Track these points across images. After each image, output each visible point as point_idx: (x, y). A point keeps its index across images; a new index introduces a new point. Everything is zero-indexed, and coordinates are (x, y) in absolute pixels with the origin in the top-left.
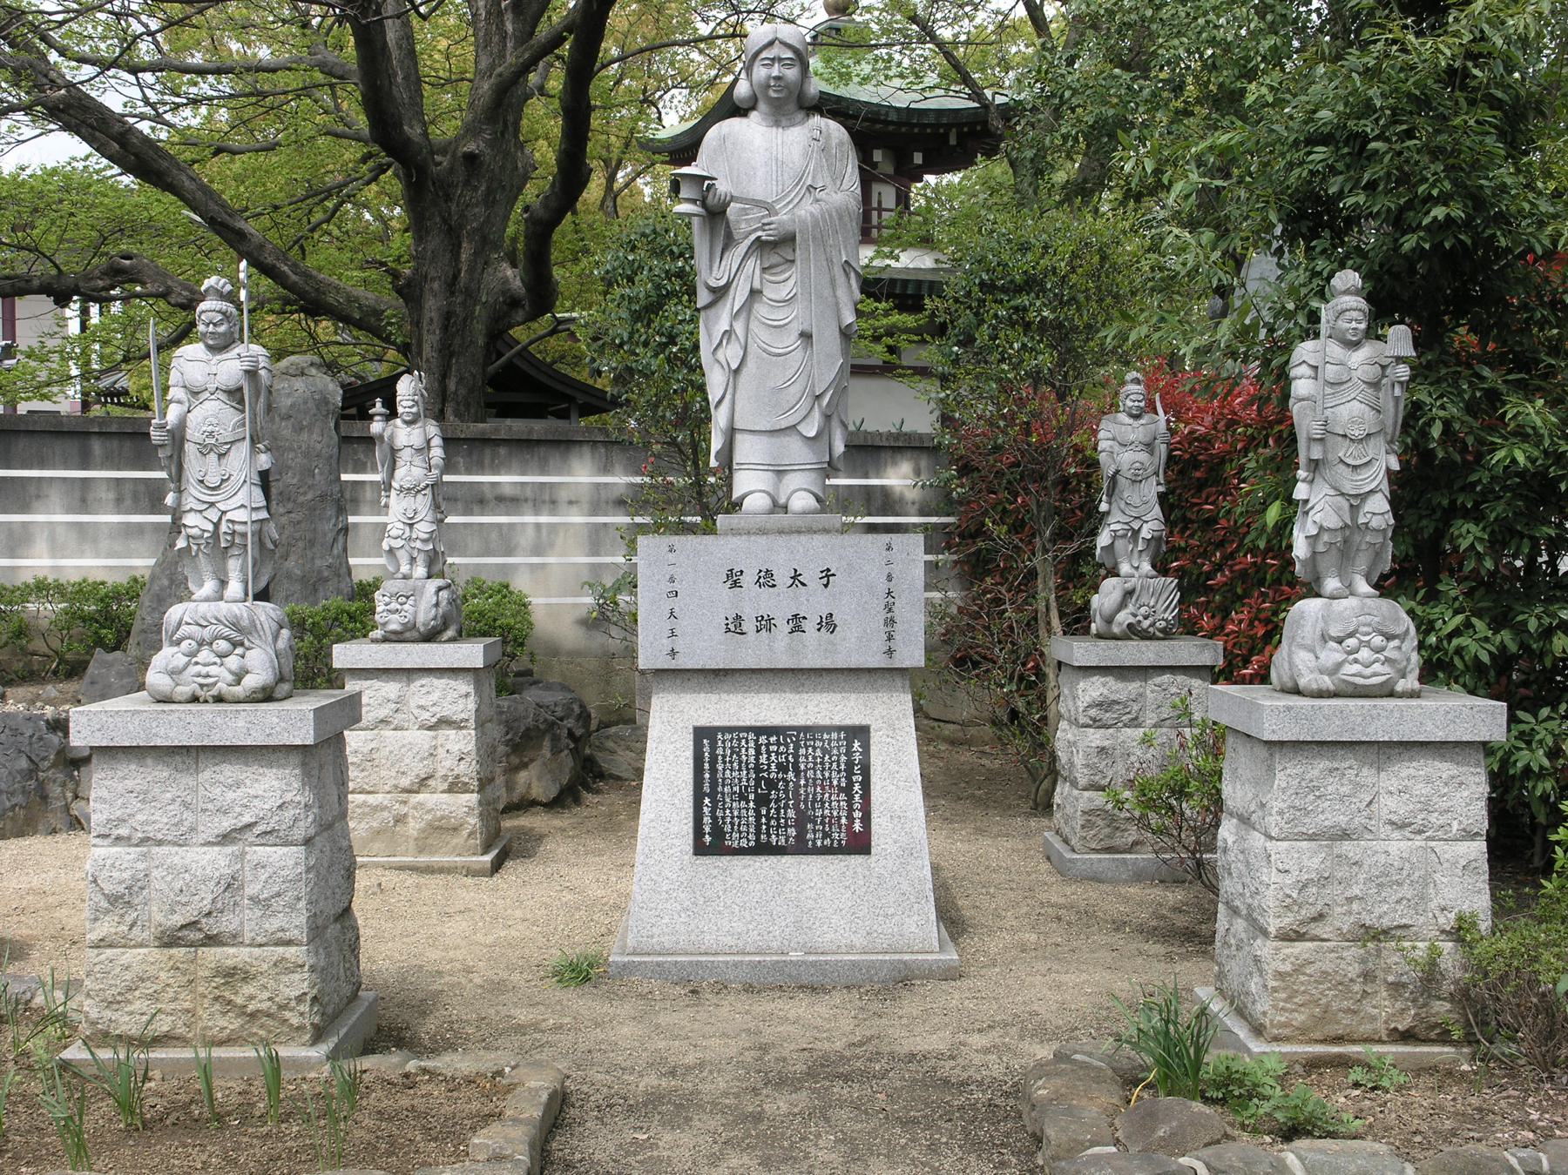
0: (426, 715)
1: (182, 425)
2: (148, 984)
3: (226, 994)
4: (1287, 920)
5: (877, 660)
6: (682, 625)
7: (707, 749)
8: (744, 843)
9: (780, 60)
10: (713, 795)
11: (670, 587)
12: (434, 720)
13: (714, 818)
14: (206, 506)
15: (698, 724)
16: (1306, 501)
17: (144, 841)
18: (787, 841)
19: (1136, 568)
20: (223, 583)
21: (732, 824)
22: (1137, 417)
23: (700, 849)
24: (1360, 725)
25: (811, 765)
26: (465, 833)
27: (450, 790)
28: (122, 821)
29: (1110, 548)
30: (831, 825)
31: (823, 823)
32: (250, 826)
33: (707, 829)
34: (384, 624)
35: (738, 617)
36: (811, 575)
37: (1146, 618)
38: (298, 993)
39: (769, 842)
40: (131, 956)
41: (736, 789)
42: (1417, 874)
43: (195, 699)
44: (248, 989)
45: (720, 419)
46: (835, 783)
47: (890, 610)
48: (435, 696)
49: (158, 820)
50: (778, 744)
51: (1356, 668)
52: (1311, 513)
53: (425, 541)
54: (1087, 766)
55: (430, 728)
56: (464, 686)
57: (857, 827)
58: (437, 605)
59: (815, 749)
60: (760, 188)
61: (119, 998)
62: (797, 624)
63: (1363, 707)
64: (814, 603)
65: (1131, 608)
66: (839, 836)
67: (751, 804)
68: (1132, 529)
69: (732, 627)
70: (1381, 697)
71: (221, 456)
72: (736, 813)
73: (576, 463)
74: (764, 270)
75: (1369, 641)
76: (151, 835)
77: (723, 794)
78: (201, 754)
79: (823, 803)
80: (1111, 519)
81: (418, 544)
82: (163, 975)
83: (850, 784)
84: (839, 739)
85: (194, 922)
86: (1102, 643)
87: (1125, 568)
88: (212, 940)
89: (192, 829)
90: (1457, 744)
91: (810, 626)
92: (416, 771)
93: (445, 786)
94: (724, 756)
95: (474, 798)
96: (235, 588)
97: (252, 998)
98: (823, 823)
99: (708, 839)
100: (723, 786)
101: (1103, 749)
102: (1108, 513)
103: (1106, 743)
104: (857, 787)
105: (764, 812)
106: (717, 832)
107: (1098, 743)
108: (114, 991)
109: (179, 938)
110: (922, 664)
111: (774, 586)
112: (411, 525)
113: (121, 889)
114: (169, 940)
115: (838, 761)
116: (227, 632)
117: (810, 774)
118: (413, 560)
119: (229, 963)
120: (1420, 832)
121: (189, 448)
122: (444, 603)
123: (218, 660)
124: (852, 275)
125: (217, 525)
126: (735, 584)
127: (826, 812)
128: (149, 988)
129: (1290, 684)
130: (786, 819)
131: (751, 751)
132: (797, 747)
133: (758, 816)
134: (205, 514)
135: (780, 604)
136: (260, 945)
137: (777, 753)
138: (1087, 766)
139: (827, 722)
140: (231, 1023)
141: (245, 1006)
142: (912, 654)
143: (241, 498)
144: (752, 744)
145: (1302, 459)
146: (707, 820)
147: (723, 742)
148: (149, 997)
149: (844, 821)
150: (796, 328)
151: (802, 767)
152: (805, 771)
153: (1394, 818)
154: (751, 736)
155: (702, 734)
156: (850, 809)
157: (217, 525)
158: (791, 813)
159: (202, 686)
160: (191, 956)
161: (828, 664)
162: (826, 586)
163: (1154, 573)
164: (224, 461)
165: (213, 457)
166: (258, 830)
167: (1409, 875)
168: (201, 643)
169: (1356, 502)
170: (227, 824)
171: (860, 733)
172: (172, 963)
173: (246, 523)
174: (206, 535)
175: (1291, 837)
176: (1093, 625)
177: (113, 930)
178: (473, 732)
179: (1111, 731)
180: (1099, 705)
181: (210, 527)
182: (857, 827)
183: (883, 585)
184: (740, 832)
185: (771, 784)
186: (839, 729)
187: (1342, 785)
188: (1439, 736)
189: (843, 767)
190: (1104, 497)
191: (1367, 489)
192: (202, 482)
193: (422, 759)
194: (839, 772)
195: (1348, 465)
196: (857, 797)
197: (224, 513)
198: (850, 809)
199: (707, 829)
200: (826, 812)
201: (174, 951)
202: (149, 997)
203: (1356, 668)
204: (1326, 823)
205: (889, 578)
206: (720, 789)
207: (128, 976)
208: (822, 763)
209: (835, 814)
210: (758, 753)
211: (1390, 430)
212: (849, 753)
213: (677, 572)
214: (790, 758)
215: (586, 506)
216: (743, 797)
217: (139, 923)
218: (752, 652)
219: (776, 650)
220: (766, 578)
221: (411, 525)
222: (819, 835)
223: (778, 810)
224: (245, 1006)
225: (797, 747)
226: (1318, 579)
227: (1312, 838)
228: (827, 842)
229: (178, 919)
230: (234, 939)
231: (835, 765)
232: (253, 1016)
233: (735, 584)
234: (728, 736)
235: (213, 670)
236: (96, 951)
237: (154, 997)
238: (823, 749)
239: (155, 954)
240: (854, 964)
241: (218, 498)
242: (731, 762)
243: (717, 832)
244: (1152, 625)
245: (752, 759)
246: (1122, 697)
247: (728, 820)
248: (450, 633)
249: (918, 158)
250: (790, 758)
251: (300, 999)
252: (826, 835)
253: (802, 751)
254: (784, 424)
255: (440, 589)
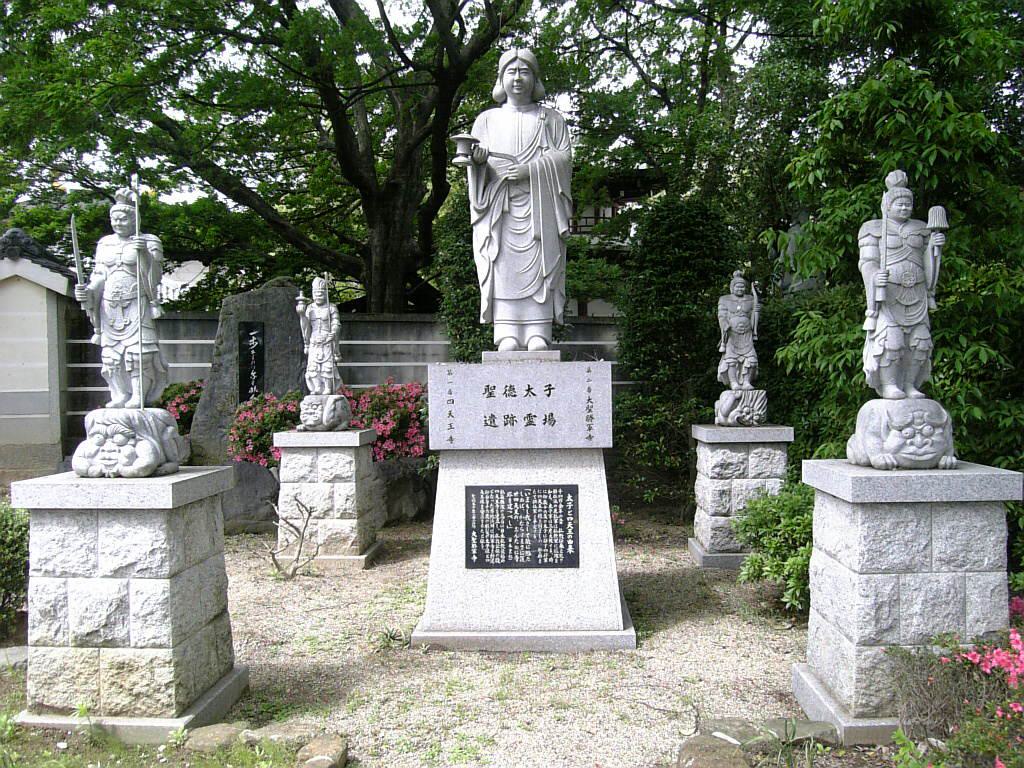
0: (327, 474)
1: (101, 287)
2: (67, 672)
3: (119, 681)
4: (867, 632)
5: (582, 443)
6: (457, 421)
7: (474, 500)
8: (498, 561)
9: (519, 70)
10: (478, 531)
11: (449, 397)
12: (332, 477)
13: (478, 544)
14: (115, 343)
15: (468, 485)
16: (873, 331)
17: (64, 574)
18: (525, 558)
19: (740, 385)
20: (129, 395)
21: (490, 549)
22: (741, 296)
23: (470, 564)
24: (920, 490)
25: (540, 511)
26: (350, 542)
27: (341, 517)
28: (47, 560)
29: (725, 373)
30: (553, 548)
31: (548, 548)
32: (133, 564)
33: (474, 552)
34: (305, 421)
35: (493, 416)
36: (540, 389)
37: (748, 413)
38: (166, 682)
39: (514, 560)
40: (57, 653)
41: (493, 526)
42: (959, 596)
43: (102, 476)
44: (134, 677)
45: (485, 292)
46: (556, 522)
47: (590, 411)
48: (332, 464)
49: (74, 560)
50: (519, 497)
51: (912, 449)
52: (877, 340)
53: (328, 373)
54: (714, 502)
55: (330, 481)
56: (348, 457)
57: (570, 550)
58: (335, 409)
59: (543, 500)
60: (505, 148)
61: (49, 681)
62: (530, 420)
63: (921, 477)
64: (540, 406)
65: (738, 408)
66: (559, 556)
67: (502, 536)
68: (739, 362)
69: (489, 422)
70: (925, 469)
71: (124, 308)
72: (492, 541)
73: (437, 334)
74: (510, 199)
75: (921, 430)
76: (67, 570)
77: (484, 529)
78: (100, 515)
79: (548, 534)
80: (727, 356)
81: (325, 375)
82: (77, 666)
83: (566, 522)
84: (558, 494)
85: (97, 631)
86: (722, 429)
87: (734, 385)
88: (110, 643)
89: (95, 567)
90: (987, 503)
91: (538, 421)
92: (322, 507)
93: (339, 515)
94: (485, 505)
95: (354, 522)
96: (137, 398)
97: (135, 684)
98: (548, 548)
99: (475, 558)
100: (484, 524)
101: (724, 491)
102: (724, 353)
103: (725, 488)
104: (570, 524)
105: (510, 540)
106: (481, 553)
107: (720, 488)
108: (45, 676)
109: (87, 641)
110: (611, 446)
111: (515, 396)
112: (321, 364)
113: (48, 607)
114: (83, 642)
115: (558, 508)
116: (122, 429)
117: (540, 516)
118: (322, 384)
119: (120, 659)
120: (961, 566)
121: (106, 304)
122: (339, 409)
123: (117, 448)
124: (566, 201)
125: (122, 356)
126: (491, 395)
127: (551, 541)
128: (68, 675)
129: (864, 460)
130: (525, 545)
131: (502, 502)
132: (531, 499)
133: (507, 544)
134: (115, 348)
135: (519, 407)
136: (142, 648)
137: (519, 503)
138: (714, 502)
139: (551, 483)
140: (123, 700)
141: (132, 690)
142: (606, 440)
143: (136, 338)
144: (502, 497)
145: (870, 303)
146: (474, 546)
147: (484, 496)
148: (67, 681)
149: (562, 546)
150: (532, 233)
151: (535, 511)
152: (537, 515)
153: (943, 556)
154: (502, 492)
155: (471, 491)
156: (566, 539)
157: (122, 356)
158: (528, 541)
159: (106, 466)
160: (96, 654)
161: (551, 445)
162: (549, 395)
163: (752, 387)
164: (126, 312)
165: (119, 309)
166: (138, 568)
167: (953, 598)
168: (106, 436)
169: (906, 332)
170: (116, 563)
171: (572, 490)
172: (82, 659)
173: (138, 354)
174: (116, 363)
175: (870, 571)
176: (716, 419)
177: (45, 635)
178: (354, 484)
179: (728, 481)
180: (722, 466)
181: (118, 357)
182: (570, 550)
183: (585, 395)
184: (495, 554)
185: (515, 523)
186: (558, 487)
187: (906, 533)
188: (976, 497)
189: (561, 511)
190: (722, 344)
191: (916, 322)
192: (112, 326)
193: (325, 499)
194: (558, 515)
195: (902, 305)
196: (570, 531)
197: (126, 347)
198: (566, 539)
199: (474, 552)
200: (551, 541)
201: (84, 650)
202: (67, 681)
203: (912, 449)
204: (895, 561)
205: (589, 390)
206: (482, 526)
207: (56, 666)
208: (547, 509)
209: (556, 541)
210: (506, 503)
211: (930, 281)
212: (564, 503)
213: (453, 387)
214: (527, 506)
215: (442, 357)
216: (497, 531)
217: (62, 630)
218: (502, 438)
219: (517, 437)
220: (510, 391)
221: (321, 364)
222: (546, 555)
223: (519, 539)
224: (132, 690)
225: (531, 499)
226: (881, 387)
227: (886, 572)
228: (551, 560)
229: (86, 629)
230: (124, 642)
231: (555, 510)
232: (138, 696)
233: (491, 395)
234: (487, 492)
235: (113, 455)
236: (34, 648)
237: (72, 681)
238: (548, 500)
239: (73, 651)
240: (568, 639)
241: (125, 337)
242: (489, 509)
243: (481, 553)
244: (752, 418)
245: (503, 507)
246: (735, 460)
247: (488, 545)
248: (344, 425)
249: (622, 194)
250: (527, 506)
251: (167, 686)
252: (550, 556)
253: (535, 501)
254: (525, 295)
255: (336, 400)
